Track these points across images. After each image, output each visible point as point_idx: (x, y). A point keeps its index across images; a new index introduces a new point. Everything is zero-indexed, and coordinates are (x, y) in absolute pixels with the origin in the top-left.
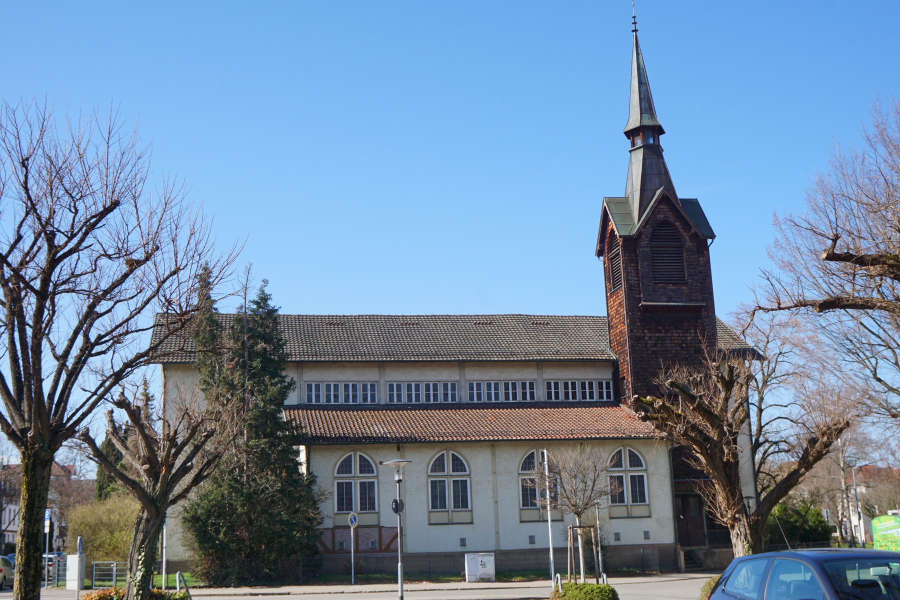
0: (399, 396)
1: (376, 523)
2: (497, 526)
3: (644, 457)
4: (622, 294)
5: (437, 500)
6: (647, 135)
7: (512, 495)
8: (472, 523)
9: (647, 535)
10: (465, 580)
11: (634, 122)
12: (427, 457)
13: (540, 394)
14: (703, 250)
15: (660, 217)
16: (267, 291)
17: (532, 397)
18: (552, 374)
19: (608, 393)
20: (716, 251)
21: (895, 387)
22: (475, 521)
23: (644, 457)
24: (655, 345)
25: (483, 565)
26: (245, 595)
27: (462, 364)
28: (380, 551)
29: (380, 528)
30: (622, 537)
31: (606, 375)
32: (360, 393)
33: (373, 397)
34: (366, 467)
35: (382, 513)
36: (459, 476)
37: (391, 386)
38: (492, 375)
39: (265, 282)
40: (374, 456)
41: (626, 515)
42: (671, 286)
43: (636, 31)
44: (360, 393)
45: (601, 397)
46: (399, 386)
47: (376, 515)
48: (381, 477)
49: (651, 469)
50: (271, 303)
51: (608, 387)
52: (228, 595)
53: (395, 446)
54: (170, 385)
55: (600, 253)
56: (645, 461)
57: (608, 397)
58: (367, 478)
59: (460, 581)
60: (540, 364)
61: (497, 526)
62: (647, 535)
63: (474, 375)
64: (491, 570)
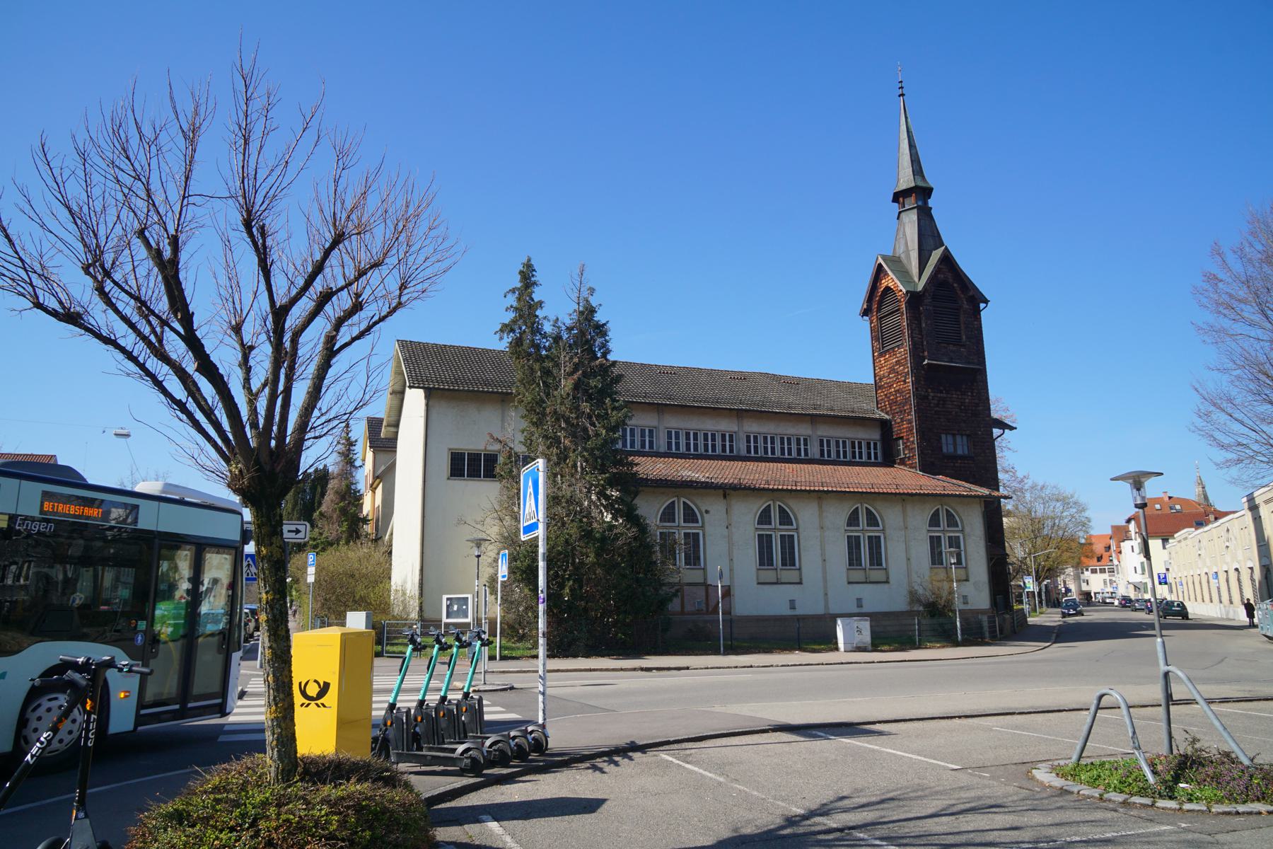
0: (677, 444)
2: (825, 587)
4: (903, 351)
5: (765, 557)
6: (917, 196)
7: (922, 551)
8: (800, 583)
9: (792, 604)
10: (837, 649)
11: (906, 180)
12: (754, 508)
13: (814, 451)
14: (977, 312)
15: (941, 276)
16: (594, 302)
17: (806, 454)
18: (825, 431)
19: (876, 454)
20: (988, 317)
24: (937, 405)
25: (860, 631)
26: (634, 669)
27: (740, 414)
28: (707, 612)
30: (864, 603)
31: (875, 435)
32: (638, 439)
33: (651, 443)
34: (690, 516)
36: (786, 531)
37: (669, 433)
38: (769, 428)
39: (592, 291)
40: (700, 505)
42: (951, 347)
43: (902, 95)
45: (869, 457)
46: (677, 434)
48: (707, 527)
49: (967, 530)
50: (600, 317)
51: (875, 448)
52: (614, 670)
53: (721, 492)
55: (865, 313)
57: (876, 458)
58: (691, 528)
60: (814, 419)
61: (825, 587)
62: (792, 604)
63: (753, 427)
64: (866, 637)
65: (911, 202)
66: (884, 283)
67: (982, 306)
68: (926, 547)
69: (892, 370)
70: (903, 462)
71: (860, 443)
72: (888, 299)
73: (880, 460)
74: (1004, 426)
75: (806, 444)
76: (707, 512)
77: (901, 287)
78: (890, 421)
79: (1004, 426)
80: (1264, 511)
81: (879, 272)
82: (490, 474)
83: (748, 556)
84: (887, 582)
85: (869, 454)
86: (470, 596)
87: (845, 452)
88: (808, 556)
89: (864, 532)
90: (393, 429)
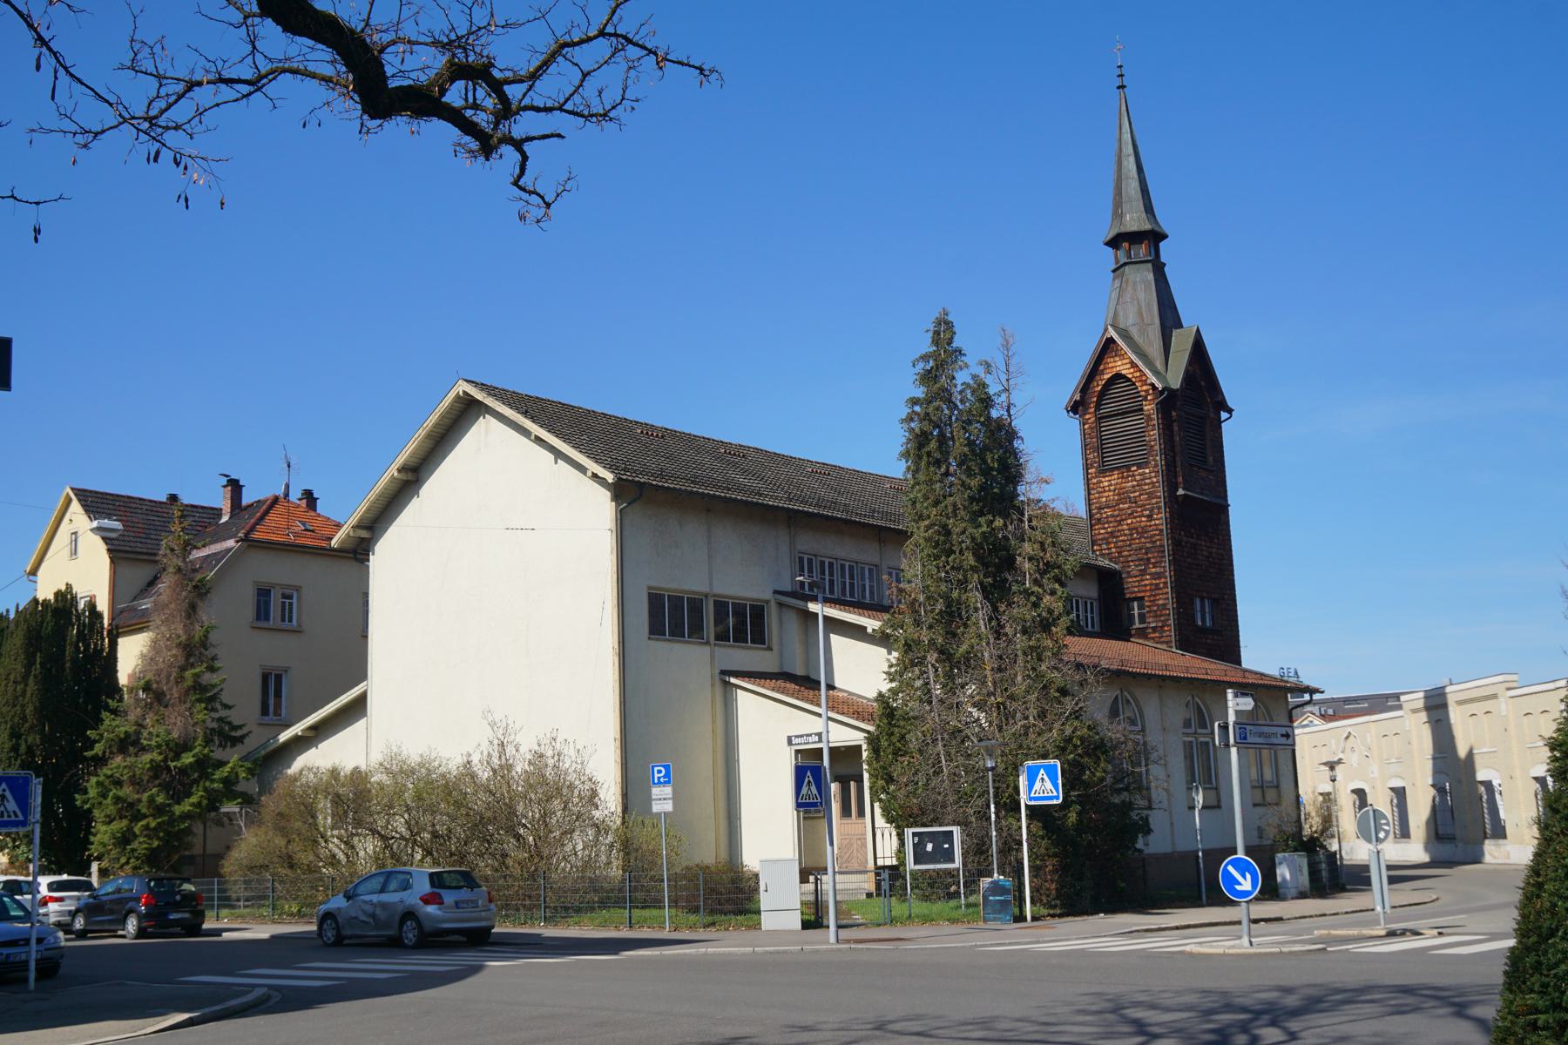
4: (1150, 476)
6: (1140, 244)
11: (1134, 221)
14: (1218, 423)
43: (1122, 87)
55: (1076, 408)
59: (749, 928)
65: (1142, 251)
66: (1119, 366)
67: (1224, 415)
69: (1123, 496)
70: (1142, 633)
72: (1116, 390)
73: (1097, 628)
77: (1154, 380)
78: (1120, 573)
80: (1456, 715)
81: (1108, 347)
82: (696, 630)
90: (364, 534)
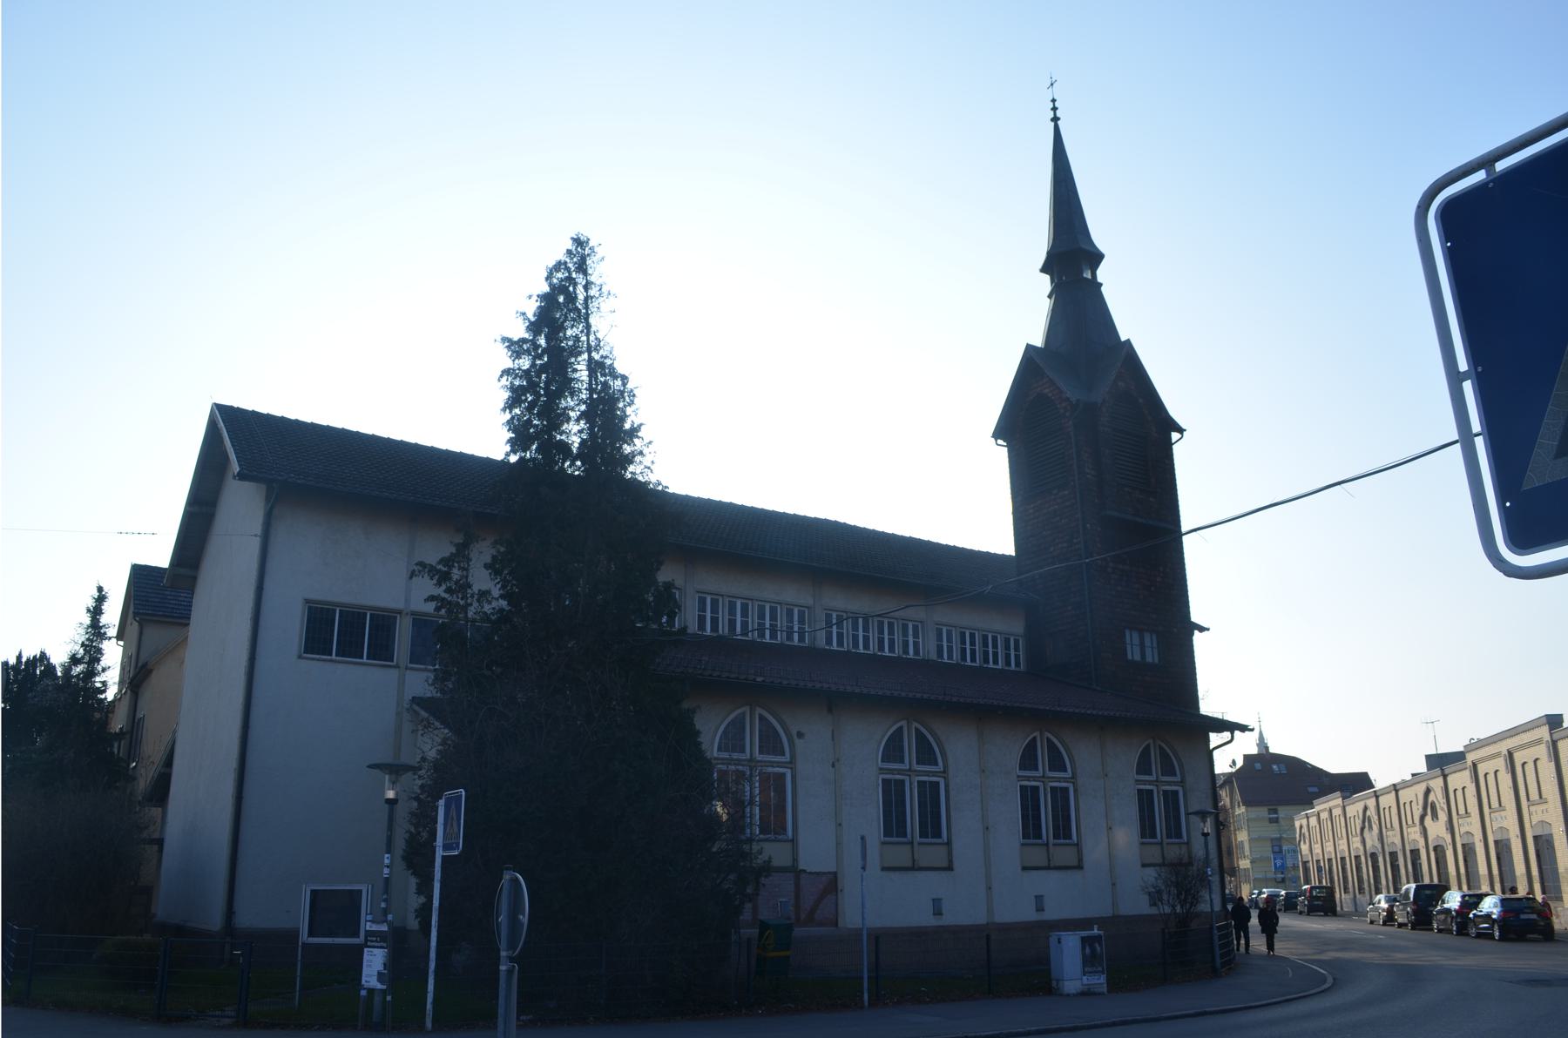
1: (789, 863)
3: (1179, 760)
8: (950, 868)
14: (1168, 447)
20: (1185, 456)
21: (87, 621)
22: (956, 864)
23: (1179, 760)
29: (795, 871)
32: (781, 622)
35: (956, 845)
41: (909, 864)
44: (753, 621)
47: (944, 849)
51: (1017, 649)
54: (384, 572)
56: (1181, 766)
67: (1175, 436)
68: (1133, 810)
71: (995, 639)
74: (1202, 629)
75: (916, 635)
76: (800, 735)
79: (1202, 629)
83: (868, 818)
84: (1080, 867)
85: (1008, 657)
86: (364, 888)
87: (973, 652)
88: (963, 824)
89: (1046, 779)
